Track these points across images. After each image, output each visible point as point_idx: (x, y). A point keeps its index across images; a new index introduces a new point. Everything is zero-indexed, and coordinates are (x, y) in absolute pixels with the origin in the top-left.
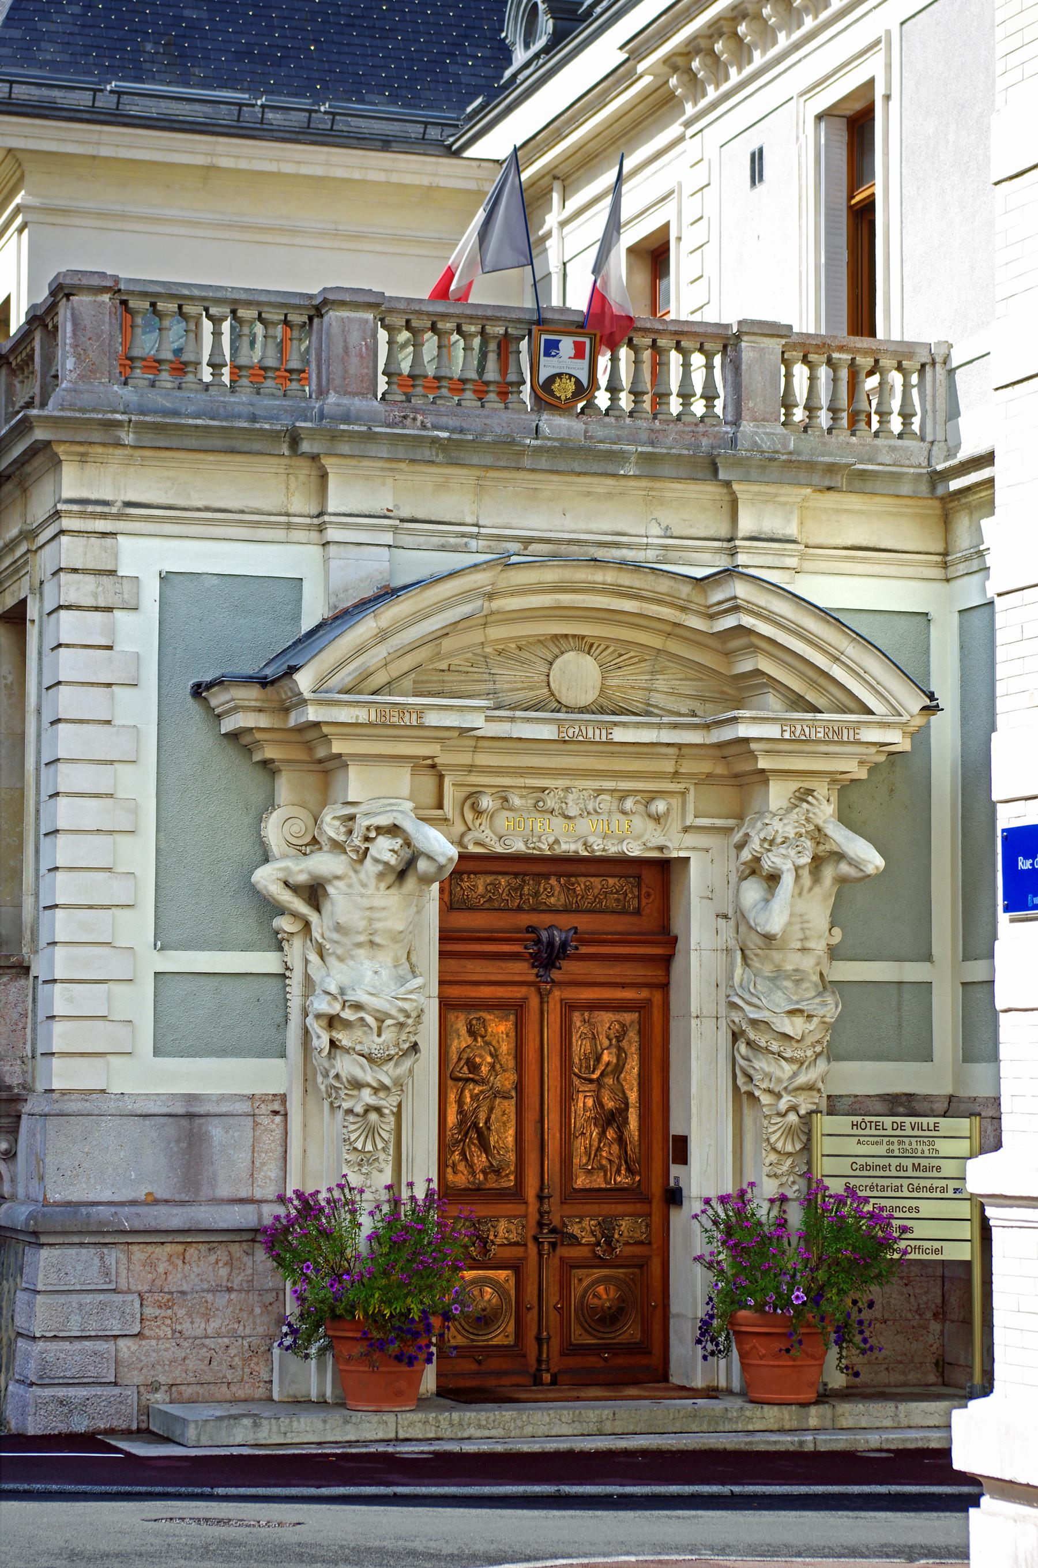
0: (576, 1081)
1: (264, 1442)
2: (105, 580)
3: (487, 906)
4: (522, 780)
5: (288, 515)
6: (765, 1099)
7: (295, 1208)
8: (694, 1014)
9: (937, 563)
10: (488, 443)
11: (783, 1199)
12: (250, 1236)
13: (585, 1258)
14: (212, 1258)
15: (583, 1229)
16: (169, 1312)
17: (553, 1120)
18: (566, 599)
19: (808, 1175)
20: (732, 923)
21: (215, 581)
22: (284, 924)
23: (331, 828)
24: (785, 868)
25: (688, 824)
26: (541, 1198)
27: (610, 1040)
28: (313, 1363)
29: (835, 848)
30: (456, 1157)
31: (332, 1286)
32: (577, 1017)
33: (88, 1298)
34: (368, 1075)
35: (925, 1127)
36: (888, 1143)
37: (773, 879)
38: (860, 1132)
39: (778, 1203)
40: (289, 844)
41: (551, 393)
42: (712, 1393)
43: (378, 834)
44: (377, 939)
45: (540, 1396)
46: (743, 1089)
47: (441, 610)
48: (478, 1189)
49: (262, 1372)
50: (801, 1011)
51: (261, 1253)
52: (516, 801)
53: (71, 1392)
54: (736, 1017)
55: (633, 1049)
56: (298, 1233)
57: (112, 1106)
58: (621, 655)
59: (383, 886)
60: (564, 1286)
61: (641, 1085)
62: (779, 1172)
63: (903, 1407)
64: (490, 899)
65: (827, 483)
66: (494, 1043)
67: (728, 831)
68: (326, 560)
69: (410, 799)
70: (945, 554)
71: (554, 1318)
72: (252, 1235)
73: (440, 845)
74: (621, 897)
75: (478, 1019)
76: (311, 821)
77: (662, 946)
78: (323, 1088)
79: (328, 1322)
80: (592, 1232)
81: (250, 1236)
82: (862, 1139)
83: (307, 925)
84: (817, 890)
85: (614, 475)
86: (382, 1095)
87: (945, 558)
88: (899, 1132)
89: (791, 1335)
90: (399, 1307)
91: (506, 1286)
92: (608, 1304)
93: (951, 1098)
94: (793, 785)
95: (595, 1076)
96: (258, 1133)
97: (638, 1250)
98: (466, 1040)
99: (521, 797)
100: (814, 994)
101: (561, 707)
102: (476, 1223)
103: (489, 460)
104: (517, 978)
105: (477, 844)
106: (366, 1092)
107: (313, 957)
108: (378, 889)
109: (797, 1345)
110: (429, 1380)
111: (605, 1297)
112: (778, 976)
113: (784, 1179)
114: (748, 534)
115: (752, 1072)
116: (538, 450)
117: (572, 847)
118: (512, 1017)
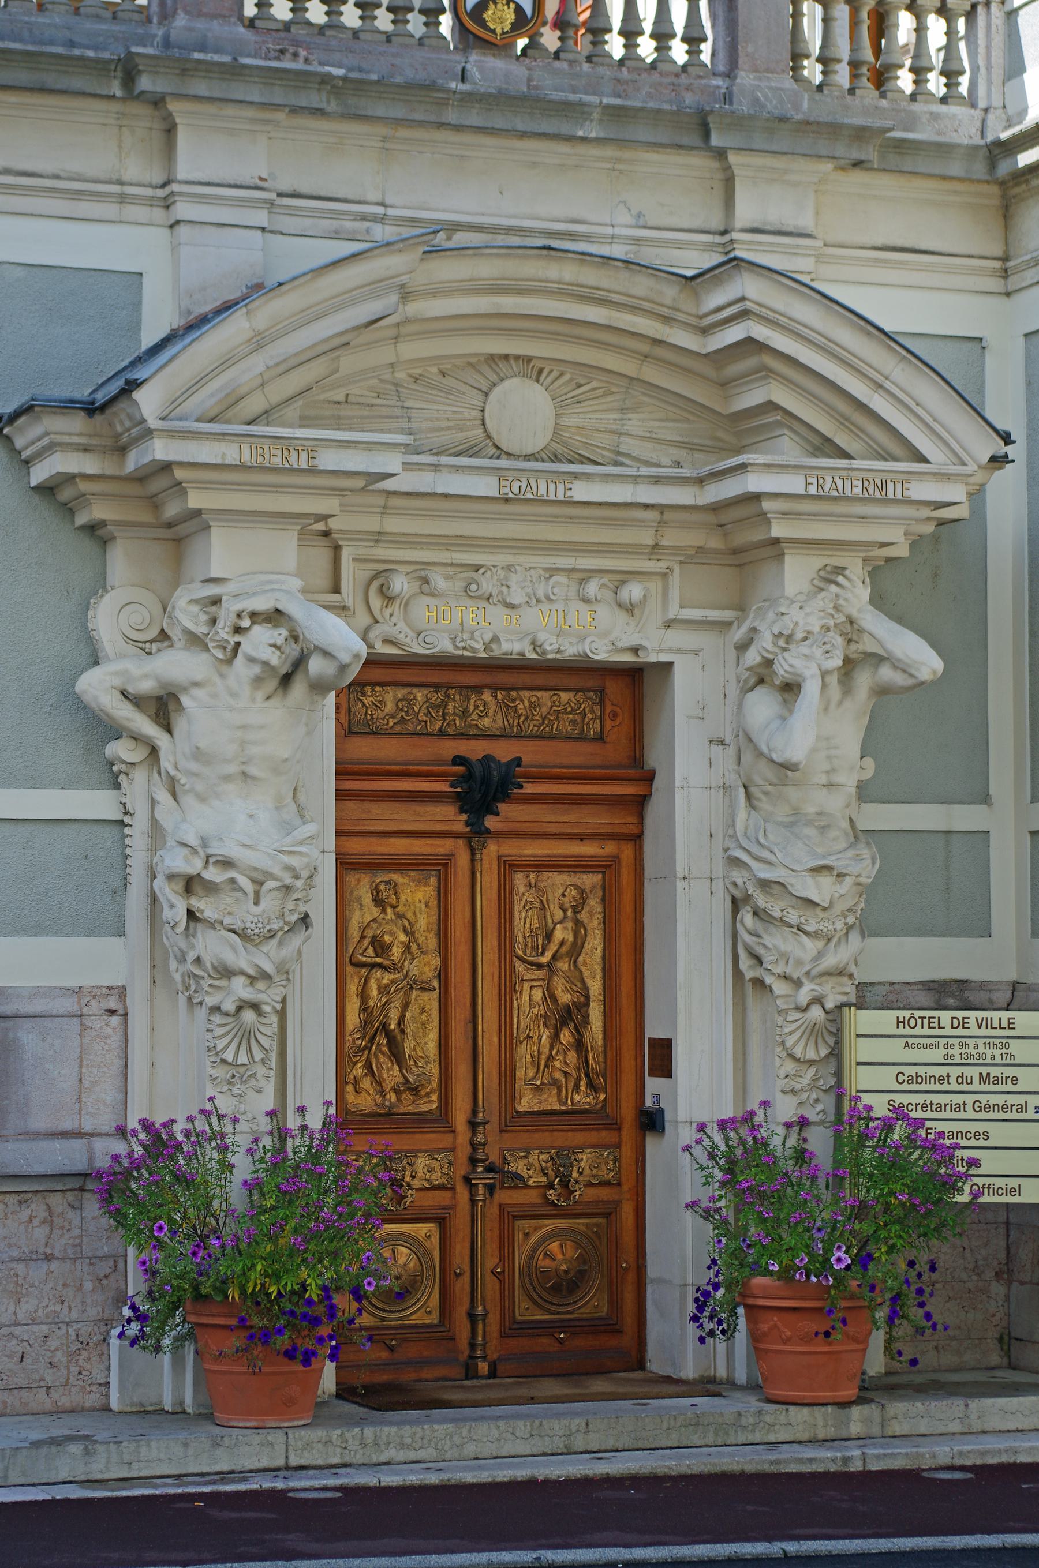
0: (520, 967)
1: (99, 1477)
3: (398, 729)
4: (448, 554)
5: (121, 183)
6: (780, 988)
7: (142, 1144)
8: (680, 875)
9: (995, 270)
10: (398, 86)
11: (803, 1122)
12: (76, 1183)
13: (534, 1205)
14: (25, 1214)
15: (530, 1166)
18: (509, 303)
19: (838, 1090)
20: (731, 751)
21: (20, 272)
22: (121, 750)
23: (188, 616)
24: (807, 673)
25: (671, 616)
26: (473, 1125)
27: (565, 911)
28: (166, 1359)
29: (871, 647)
30: (359, 1070)
31: (194, 1254)
32: (519, 880)
34: (241, 958)
35: (996, 1024)
36: (947, 1046)
37: (790, 689)
38: (908, 1031)
39: (796, 1128)
40: (128, 639)
41: (483, 24)
42: (709, 1386)
43: (253, 623)
44: (253, 770)
45: (479, 1396)
46: (749, 975)
47: (339, 308)
48: (389, 1114)
49: (95, 1371)
50: (828, 868)
51: (92, 1205)
52: (439, 582)
54: (739, 876)
55: (595, 922)
56: (143, 1181)
58: (579, 386)
59: (260, 695)
60: (505, 1243)
62: (798, 1087)
63: (974, 1404)
65: (856, 155)
66: (409, 915)
67: (724, 626)
68: (175, 247)
69: (298, 575)
70: (1005, 259)
71: (490, 1287)
72: (79, 1181)
73: (342, 639)
74: (578, 718)
75: (388, 883)
76: (157, 609)
77: (631, 786)
78: (177, 977)
79: (188, 1304)
80: (542, 1170)
81: (76, 1183)
82: (911, 1041)
83: (154, 752)
84: (848, 703)
85: (570, 139)
86: (261, 985)
87: (1004, 267)
88: (960, 1031)
89: (830, 1312)
90: (290, 1283)
91: (427, 1244)
92: (564, 1267)
93: (1015, 985)
94: (815, 562)
95: (544, 960)
96: (86, 1041)
97: (604, 1193)
99: (447, 578)
100: (844, 845)
101: (500, 452)
102: (387, 1158)
103: (399, 111)
104: (439, 827)
105: (387, 641)
106: (239, 982)
107: (163, 796)
108: (253, 700)
109: (838, 1325)
110: (328, 1376)
111: (560, 1257)
112: (796, 820)
113: (804, 1096)
115: (760, 951)
116: (469, 99)
118: (433, 881)
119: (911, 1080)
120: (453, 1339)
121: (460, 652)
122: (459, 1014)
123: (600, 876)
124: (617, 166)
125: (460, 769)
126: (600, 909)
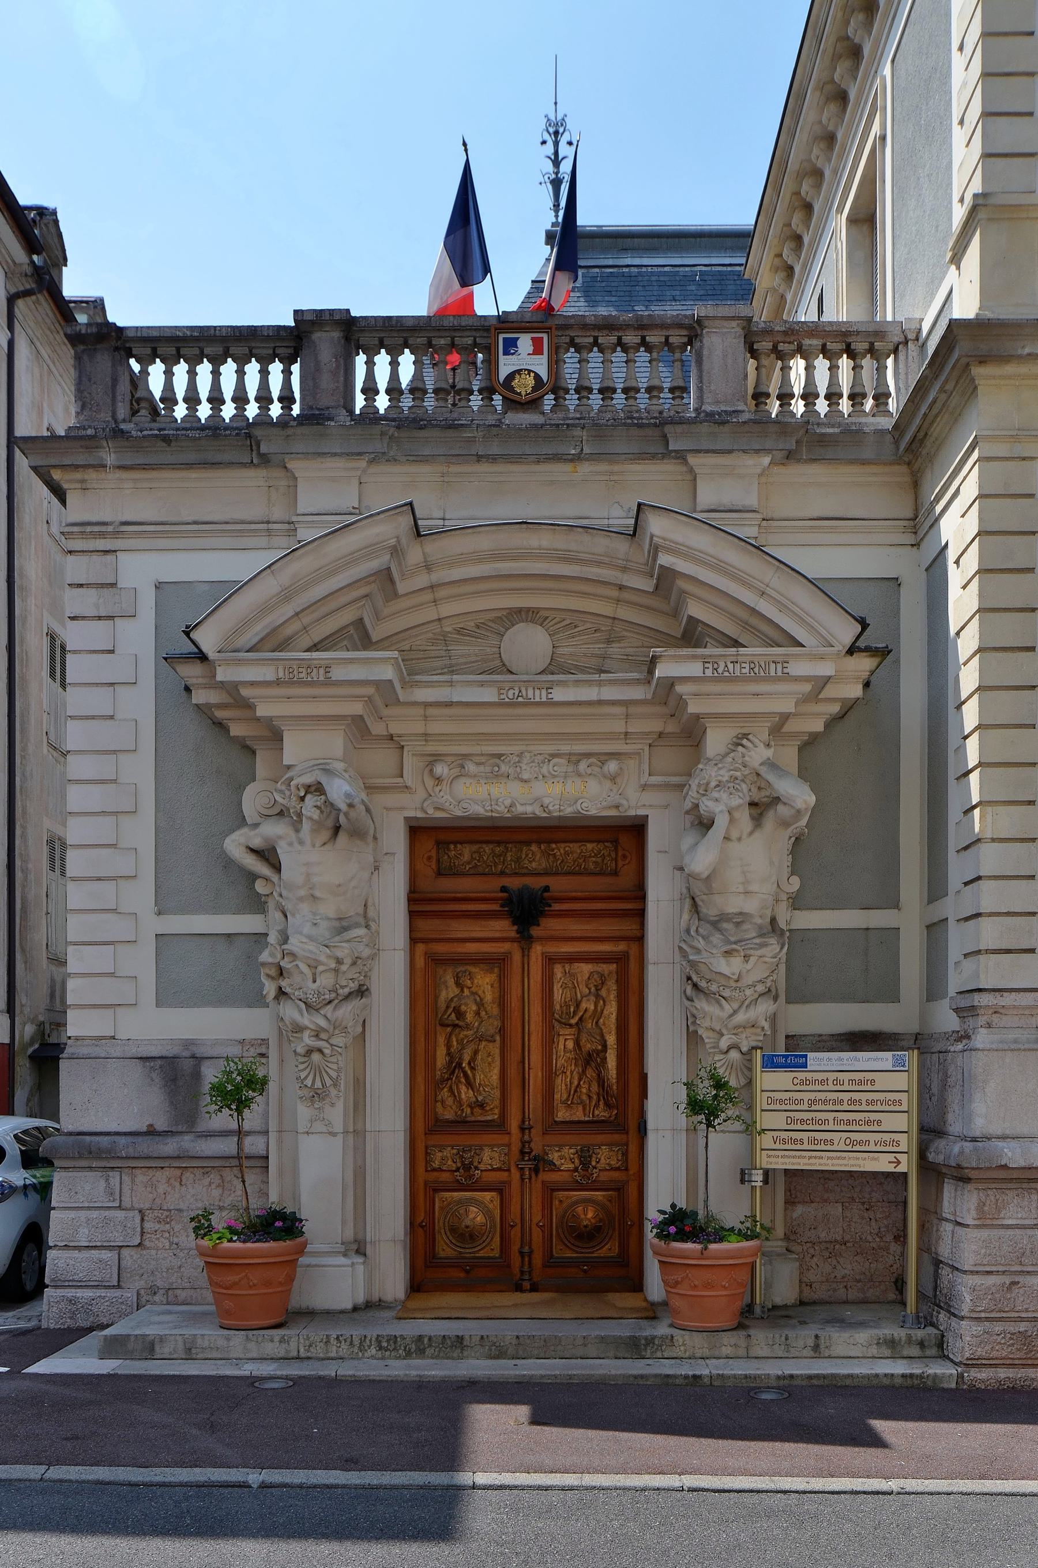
0: (556, 1024)
2: (106, 591)
16: (168, 1226)
17: (535, 1058)
24: (717, 810)
27: (590, 989)
32: (558, 970)
33: (95, 1214)
34: (306, 1020)
41: (512, 390)
44: (318, 894)
53: (80, 1293)
55: (612, 997)
57: (117, 1051)
61: (618, 1028)
64: (476, 866)
66: (480, 992)
67: (680, 787)
74: (599, 860)
91: (491, 1206)
98: (453, 991)
104: (497, 935)
105: (437, 809)
114: (707, 508)
117: (529, 809)
118: (496, 970)
119: (802, 1083)
120: (509, 1266)
121: (490, 814)
122: (514, 1057)
123: (615, 965)
124: (612, 478)
125: (505, 895)
126: (615, 988)
